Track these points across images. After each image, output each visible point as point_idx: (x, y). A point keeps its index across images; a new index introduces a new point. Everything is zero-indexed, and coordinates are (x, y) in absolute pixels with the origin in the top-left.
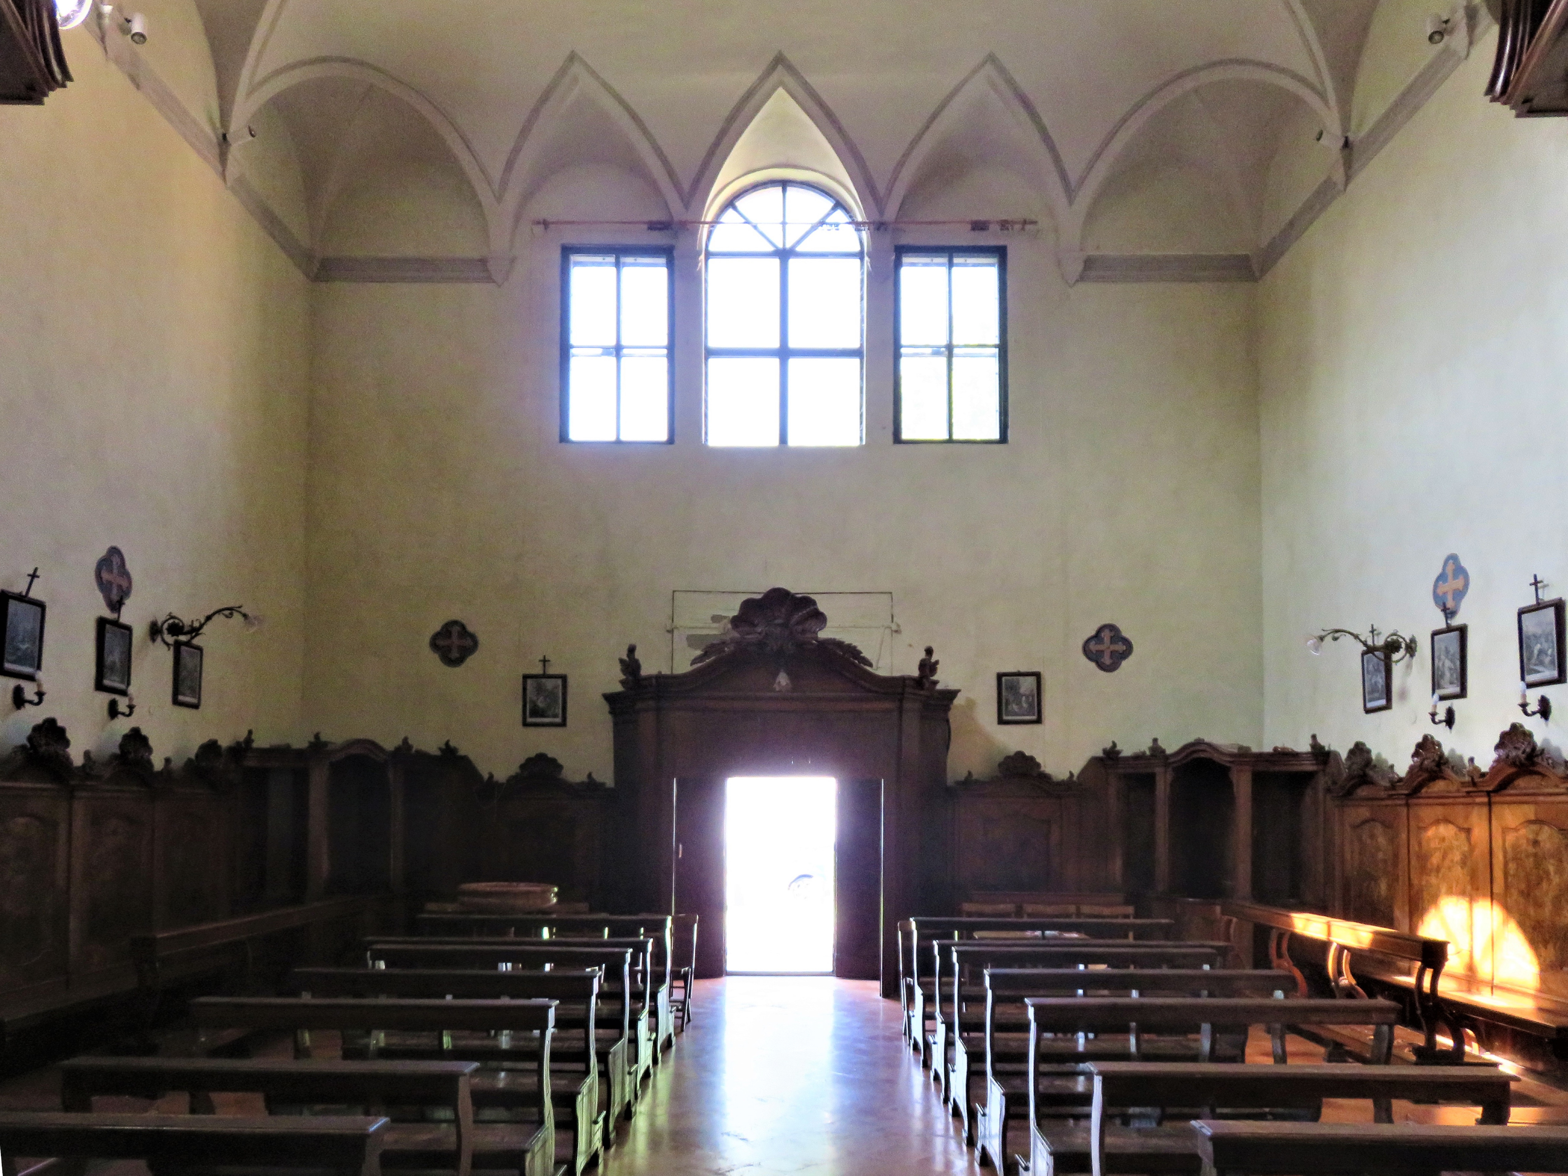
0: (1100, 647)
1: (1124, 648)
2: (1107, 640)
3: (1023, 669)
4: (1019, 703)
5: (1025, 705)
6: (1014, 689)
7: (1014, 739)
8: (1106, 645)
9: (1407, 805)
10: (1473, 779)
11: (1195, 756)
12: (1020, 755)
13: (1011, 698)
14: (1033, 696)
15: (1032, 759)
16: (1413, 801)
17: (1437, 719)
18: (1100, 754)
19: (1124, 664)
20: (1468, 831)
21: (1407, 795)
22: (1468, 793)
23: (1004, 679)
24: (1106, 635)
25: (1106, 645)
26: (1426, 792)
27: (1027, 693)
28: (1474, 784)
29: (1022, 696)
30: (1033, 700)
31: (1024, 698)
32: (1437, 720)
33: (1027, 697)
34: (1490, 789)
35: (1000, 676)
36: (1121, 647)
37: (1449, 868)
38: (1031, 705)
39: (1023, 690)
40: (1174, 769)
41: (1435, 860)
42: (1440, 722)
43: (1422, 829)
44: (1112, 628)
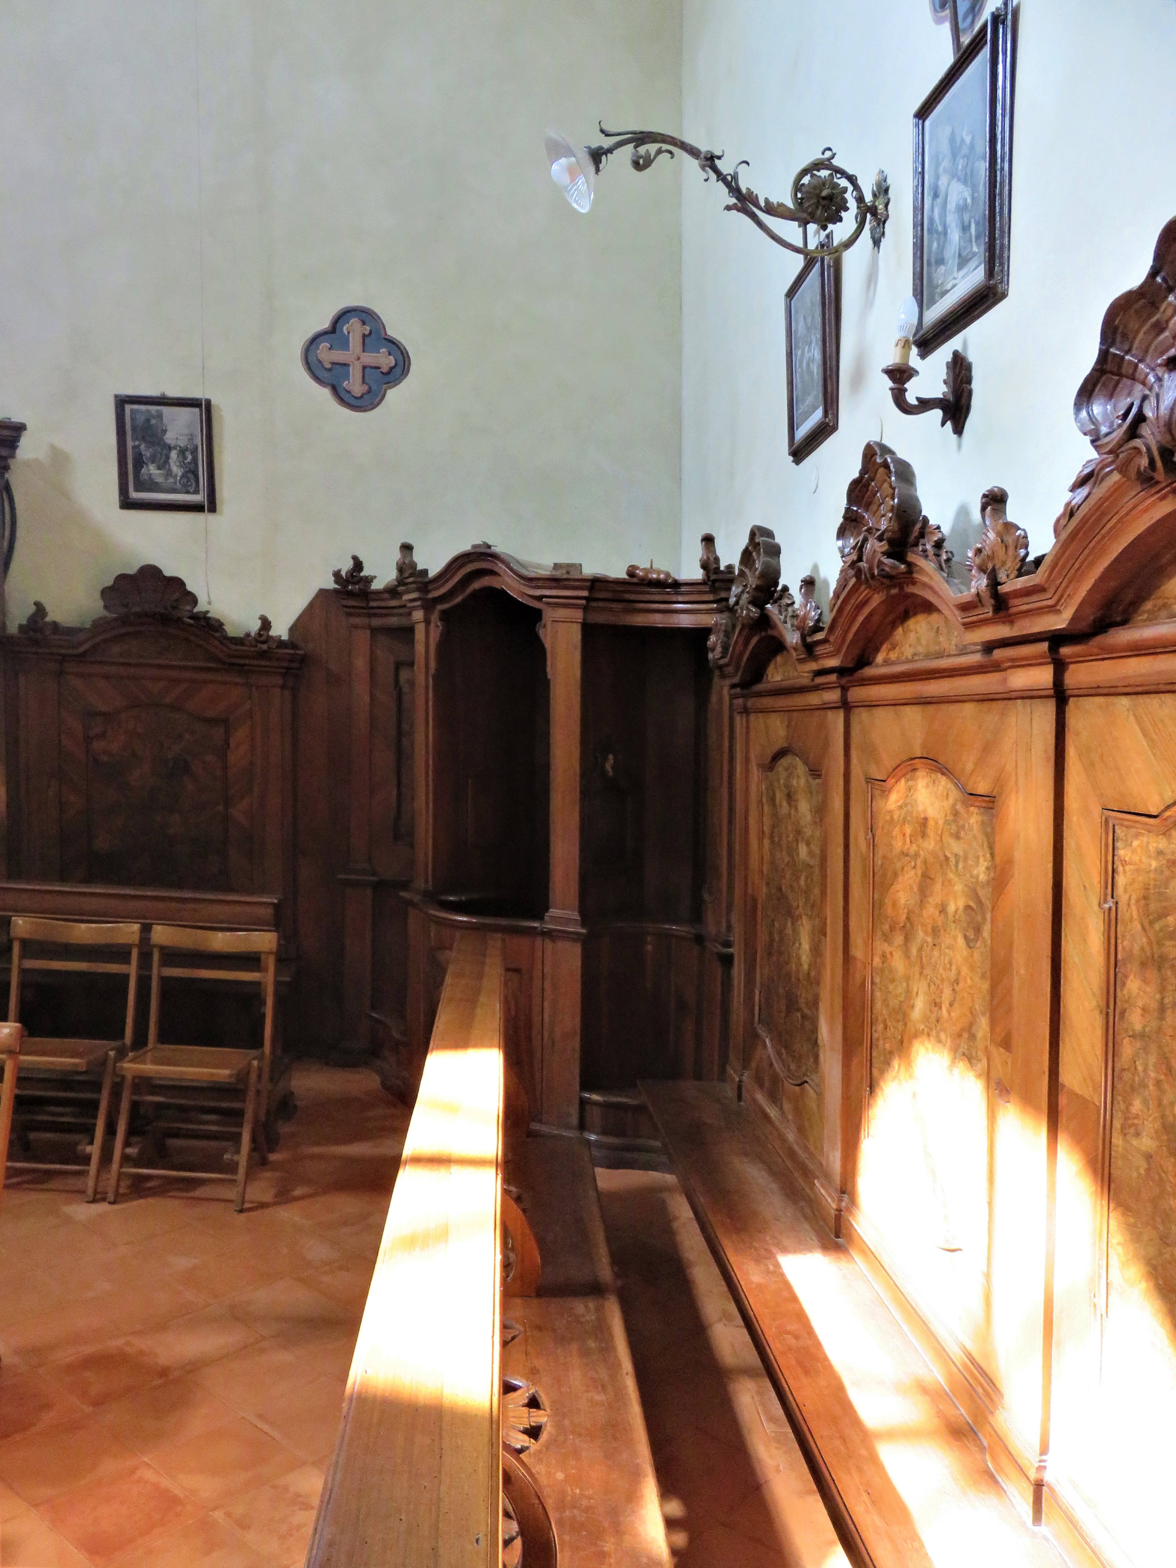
0: (338, 356)
1: (391, 361)
2: (355, 341)
3: (173, 392)
4: (164, 464)
5: (177, 470)
6: (150, 433)
7: (157, 541)
8: (353, 354)
9: (846, 706)
10: (994, 583)
11: (477, 585)
12: (151, 573)
13: (147, 453)
14: (194, 451)
15: (178, 583)
16: (857, 694)
17: (914, 391)
18: (330, 584)
19: (392, 395)
20: (990, 803)
21: (840, 671)
22: (989, 647)
23: (128, 408)
24: (354, 329)
25: (353, 354)
26: (887, 662)
27: (182, 444)
28: (1001, 604)
29: (170, 448)
30: (195, 460)
31: (174, 454)
32: (911, 399)
33: (182, 452)
34: (1060, 622)
35: (122, 402)
36: (385, 360)
37: (935, 931)
38: (192, 472)
39: (170, 437)
40: (445, 616)
41: (903, 893)
42: (925, 405)
43: (878, 785)
44: (365, 315)
